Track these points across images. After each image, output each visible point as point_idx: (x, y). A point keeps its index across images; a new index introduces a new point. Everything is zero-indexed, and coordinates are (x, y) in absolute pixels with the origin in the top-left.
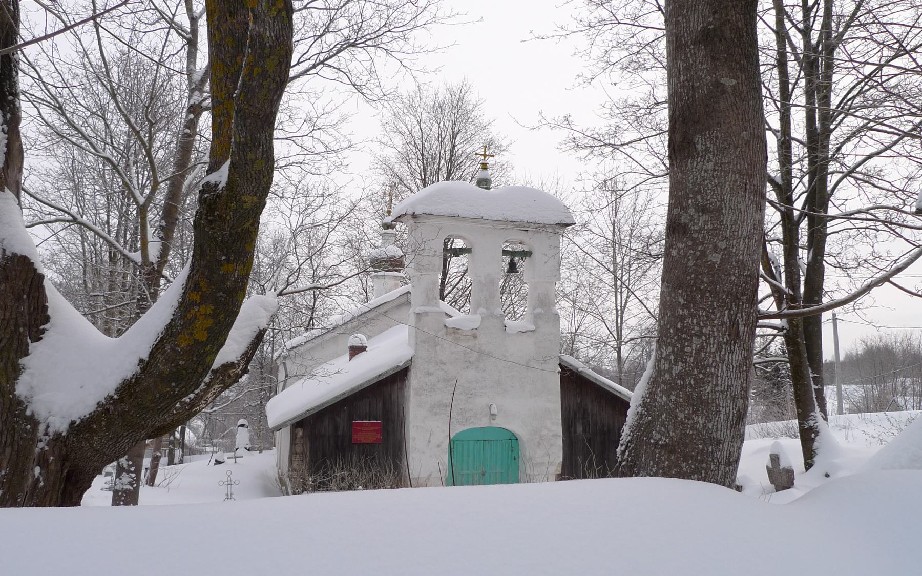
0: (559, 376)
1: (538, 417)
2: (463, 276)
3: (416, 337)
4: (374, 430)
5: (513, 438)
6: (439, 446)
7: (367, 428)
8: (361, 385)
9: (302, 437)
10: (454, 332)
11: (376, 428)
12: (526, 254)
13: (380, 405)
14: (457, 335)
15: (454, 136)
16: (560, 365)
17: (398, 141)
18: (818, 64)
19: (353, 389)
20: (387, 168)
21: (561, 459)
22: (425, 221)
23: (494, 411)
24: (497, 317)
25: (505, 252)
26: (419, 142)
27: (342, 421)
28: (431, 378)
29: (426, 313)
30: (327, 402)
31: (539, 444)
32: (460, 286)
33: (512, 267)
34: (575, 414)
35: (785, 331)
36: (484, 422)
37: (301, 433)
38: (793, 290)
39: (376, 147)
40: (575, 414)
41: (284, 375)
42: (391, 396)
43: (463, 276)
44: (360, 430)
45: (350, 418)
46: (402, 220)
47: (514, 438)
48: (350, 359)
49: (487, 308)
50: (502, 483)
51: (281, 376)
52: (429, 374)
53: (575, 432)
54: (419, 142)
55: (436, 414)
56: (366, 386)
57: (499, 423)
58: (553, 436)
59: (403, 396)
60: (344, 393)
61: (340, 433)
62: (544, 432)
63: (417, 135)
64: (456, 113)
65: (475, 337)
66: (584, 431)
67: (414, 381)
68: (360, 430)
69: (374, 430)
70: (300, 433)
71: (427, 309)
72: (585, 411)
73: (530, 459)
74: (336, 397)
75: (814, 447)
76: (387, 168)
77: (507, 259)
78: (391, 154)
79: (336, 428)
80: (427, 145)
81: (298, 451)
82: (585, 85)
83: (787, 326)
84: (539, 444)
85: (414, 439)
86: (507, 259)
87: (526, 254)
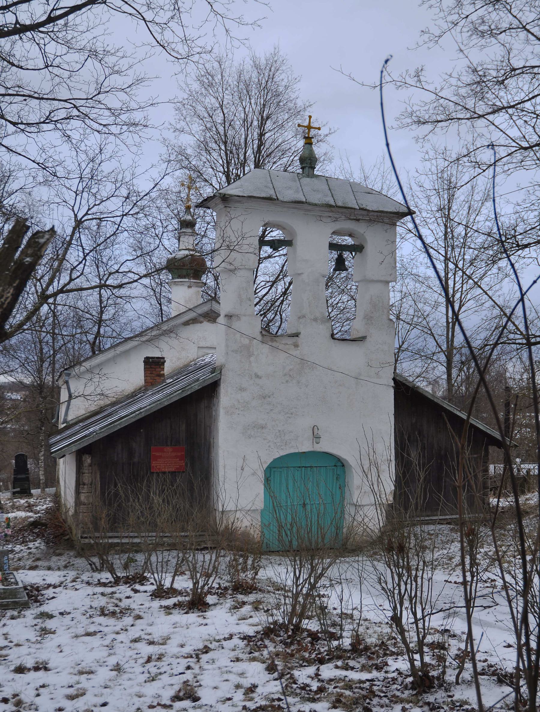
0: (392, 391)
2: (272, 286)
3: (227, 346)
9: (90, 465)
12: (358, 249)
13: (184, 427)
15: (263, 121)
16: (394, 379)
17: (197, 127)
18: (225, 467)
20: (181, 157)
22: (237, 205)
25: (333, 246)
26: (221, 129)
32: (268, 298)
33: (340, 265)
37: (89, 461)
39: (170, 135)
41: (67, 395)
43: (272, 286)
44: (160, 457)
46: (209, 204)
51: (64, 396)
52: (242, 389)
54: (221, 129)
55: (250, 437)
57: (324, 446)
59: (211, 416)
63: (219, 118)
64: (266, 93)
67: (226, 398)
68: (160, 457)
70: (87, 460)
76: (181, 157)
77: (335, 255)
78: (188, 142)
80: (230, 133)
81: (86, 481)
82: (431, 44)
86: (335, 255)
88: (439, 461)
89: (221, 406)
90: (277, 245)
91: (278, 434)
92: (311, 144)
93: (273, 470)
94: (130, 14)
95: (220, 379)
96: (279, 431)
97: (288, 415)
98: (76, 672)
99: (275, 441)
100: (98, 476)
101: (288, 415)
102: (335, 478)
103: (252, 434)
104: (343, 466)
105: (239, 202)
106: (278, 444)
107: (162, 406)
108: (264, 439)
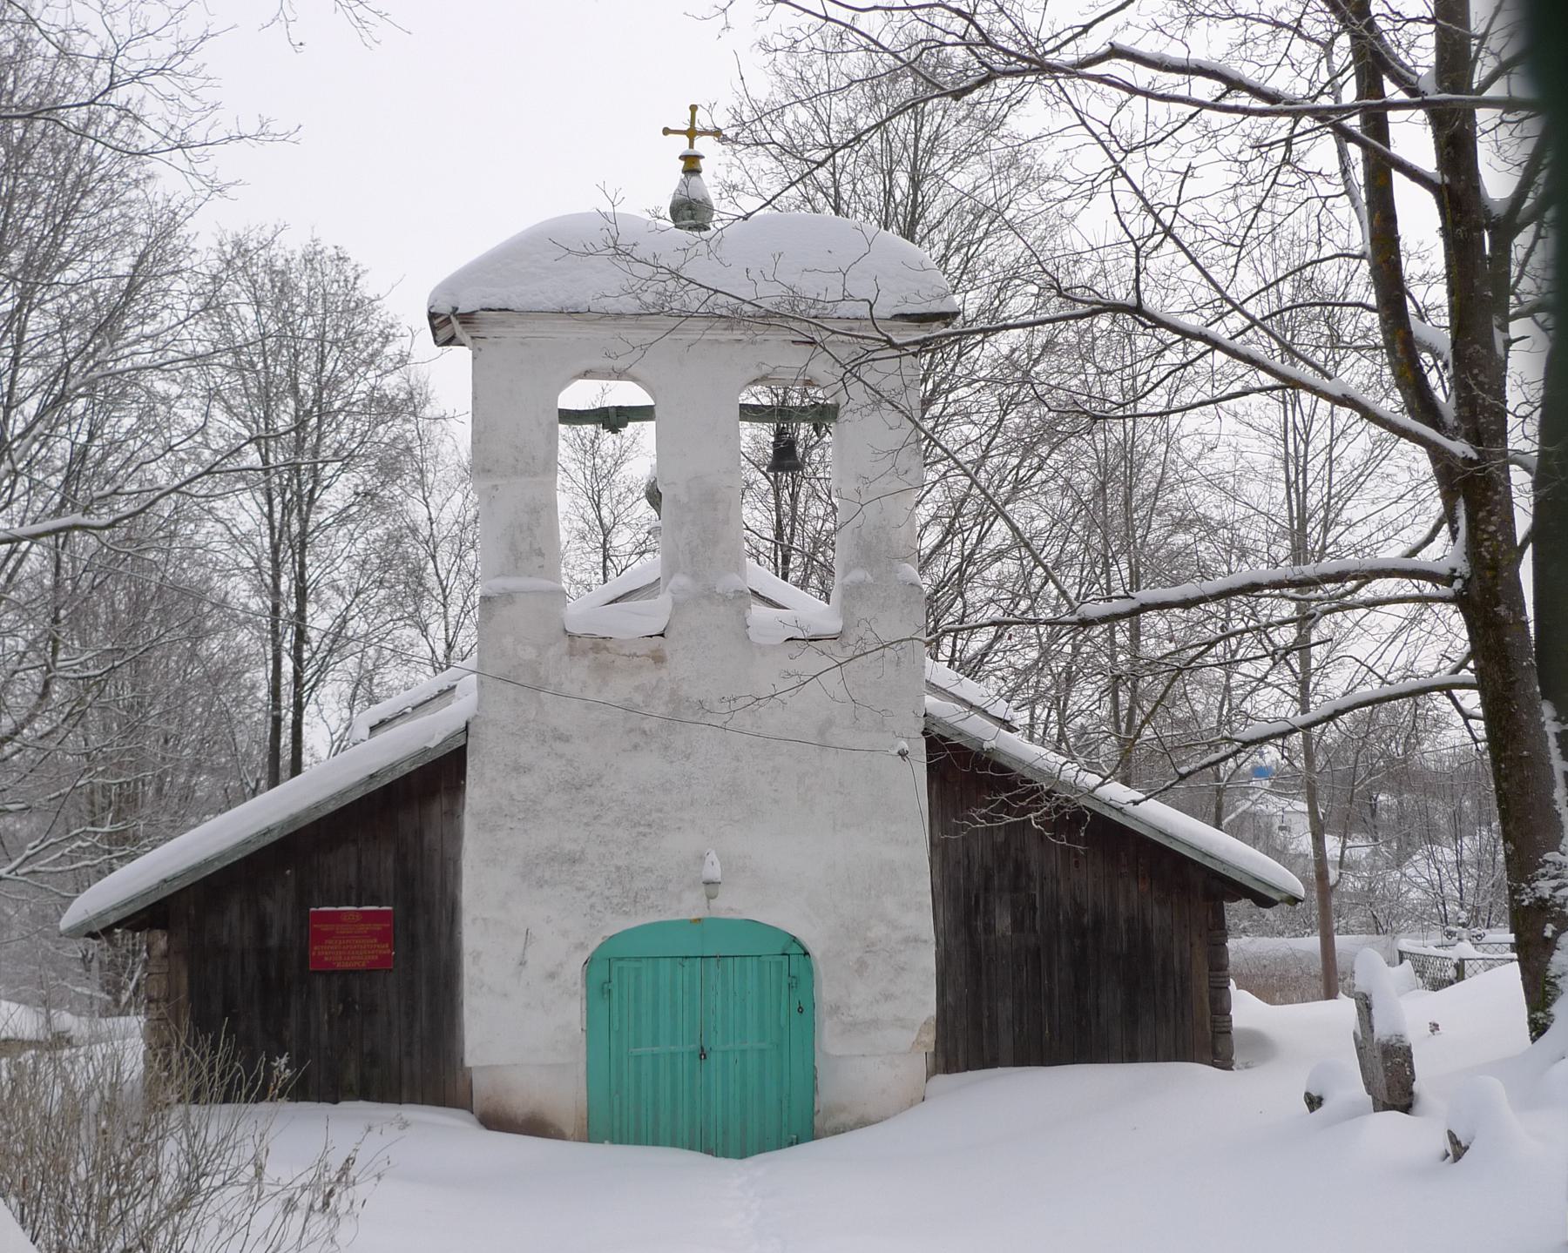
1: (860, 892)
4: (371, 934)
5: (795, 949)
6: (552, 976)
7: (350, 928)
8: (317, 806)
9: (165, 956)
10: (596, 648)
11: (378, 927)
13: (389, 863)
14: (603, 656)
19: (294, 819)
21: (932, 1010)
22: (498, 331)
23: (713, 871)
24: (725, 599)
25: (750, 413)
27: (278, 908)
28: (525, 780)
29: (509, 597)
30: (221, 856)
31: (862, 965)
33: (785, 458)
34: (988, 878)
35: (1458, 585)
36: (690, 906)
38: (1475, 438)
40: (988, 878)
42: (419, 834)
44: (331, 934)
45: (303, 902)
47: (795, 952)
48: (962, 773)
49: (694, 576)
50: (1169, 1060)
52: (520, 769)
53: (989, 928)
55: (541, 883)
56: (332, 808)
57: (735, 904)
58: (906, 940)
60: (269, 831)
61: (273, 941)
62: (878, 931)
65: (658, 659)
66: (1017, 925)
67: (480, 790)
68: (331, 934)
69: (371, 934)
71: (512, 583)
72: (1020, 869)
73: (835, 1009)
74: (247, 842)
75: (1553, 970)
79: (262, 928)
83: (1464, 568)
84: (862, 965)
85: (477, 956)
87: (823, 415)
88: (1077, 942)
89: (467, 808)
90: (613, 417)
91: (614, 876)
92: (697, 172)
93: (616, 965)
94: (1086, 28)
95: (465, 746)
96: (618, 868)
97: (641, 829)
98: (1382, 1031)
99: (607, 893)
100: (184, 981)
101: (641, 829)
102: (785, 985)
103: (547, 875)
104: (806, 953)
105: (501, 323)
106: (615, 901)
107: (320, 815)
108: (578, 889)
